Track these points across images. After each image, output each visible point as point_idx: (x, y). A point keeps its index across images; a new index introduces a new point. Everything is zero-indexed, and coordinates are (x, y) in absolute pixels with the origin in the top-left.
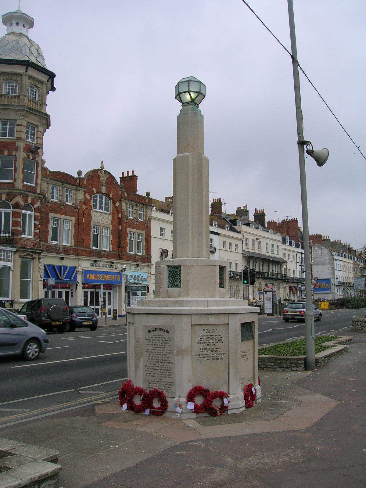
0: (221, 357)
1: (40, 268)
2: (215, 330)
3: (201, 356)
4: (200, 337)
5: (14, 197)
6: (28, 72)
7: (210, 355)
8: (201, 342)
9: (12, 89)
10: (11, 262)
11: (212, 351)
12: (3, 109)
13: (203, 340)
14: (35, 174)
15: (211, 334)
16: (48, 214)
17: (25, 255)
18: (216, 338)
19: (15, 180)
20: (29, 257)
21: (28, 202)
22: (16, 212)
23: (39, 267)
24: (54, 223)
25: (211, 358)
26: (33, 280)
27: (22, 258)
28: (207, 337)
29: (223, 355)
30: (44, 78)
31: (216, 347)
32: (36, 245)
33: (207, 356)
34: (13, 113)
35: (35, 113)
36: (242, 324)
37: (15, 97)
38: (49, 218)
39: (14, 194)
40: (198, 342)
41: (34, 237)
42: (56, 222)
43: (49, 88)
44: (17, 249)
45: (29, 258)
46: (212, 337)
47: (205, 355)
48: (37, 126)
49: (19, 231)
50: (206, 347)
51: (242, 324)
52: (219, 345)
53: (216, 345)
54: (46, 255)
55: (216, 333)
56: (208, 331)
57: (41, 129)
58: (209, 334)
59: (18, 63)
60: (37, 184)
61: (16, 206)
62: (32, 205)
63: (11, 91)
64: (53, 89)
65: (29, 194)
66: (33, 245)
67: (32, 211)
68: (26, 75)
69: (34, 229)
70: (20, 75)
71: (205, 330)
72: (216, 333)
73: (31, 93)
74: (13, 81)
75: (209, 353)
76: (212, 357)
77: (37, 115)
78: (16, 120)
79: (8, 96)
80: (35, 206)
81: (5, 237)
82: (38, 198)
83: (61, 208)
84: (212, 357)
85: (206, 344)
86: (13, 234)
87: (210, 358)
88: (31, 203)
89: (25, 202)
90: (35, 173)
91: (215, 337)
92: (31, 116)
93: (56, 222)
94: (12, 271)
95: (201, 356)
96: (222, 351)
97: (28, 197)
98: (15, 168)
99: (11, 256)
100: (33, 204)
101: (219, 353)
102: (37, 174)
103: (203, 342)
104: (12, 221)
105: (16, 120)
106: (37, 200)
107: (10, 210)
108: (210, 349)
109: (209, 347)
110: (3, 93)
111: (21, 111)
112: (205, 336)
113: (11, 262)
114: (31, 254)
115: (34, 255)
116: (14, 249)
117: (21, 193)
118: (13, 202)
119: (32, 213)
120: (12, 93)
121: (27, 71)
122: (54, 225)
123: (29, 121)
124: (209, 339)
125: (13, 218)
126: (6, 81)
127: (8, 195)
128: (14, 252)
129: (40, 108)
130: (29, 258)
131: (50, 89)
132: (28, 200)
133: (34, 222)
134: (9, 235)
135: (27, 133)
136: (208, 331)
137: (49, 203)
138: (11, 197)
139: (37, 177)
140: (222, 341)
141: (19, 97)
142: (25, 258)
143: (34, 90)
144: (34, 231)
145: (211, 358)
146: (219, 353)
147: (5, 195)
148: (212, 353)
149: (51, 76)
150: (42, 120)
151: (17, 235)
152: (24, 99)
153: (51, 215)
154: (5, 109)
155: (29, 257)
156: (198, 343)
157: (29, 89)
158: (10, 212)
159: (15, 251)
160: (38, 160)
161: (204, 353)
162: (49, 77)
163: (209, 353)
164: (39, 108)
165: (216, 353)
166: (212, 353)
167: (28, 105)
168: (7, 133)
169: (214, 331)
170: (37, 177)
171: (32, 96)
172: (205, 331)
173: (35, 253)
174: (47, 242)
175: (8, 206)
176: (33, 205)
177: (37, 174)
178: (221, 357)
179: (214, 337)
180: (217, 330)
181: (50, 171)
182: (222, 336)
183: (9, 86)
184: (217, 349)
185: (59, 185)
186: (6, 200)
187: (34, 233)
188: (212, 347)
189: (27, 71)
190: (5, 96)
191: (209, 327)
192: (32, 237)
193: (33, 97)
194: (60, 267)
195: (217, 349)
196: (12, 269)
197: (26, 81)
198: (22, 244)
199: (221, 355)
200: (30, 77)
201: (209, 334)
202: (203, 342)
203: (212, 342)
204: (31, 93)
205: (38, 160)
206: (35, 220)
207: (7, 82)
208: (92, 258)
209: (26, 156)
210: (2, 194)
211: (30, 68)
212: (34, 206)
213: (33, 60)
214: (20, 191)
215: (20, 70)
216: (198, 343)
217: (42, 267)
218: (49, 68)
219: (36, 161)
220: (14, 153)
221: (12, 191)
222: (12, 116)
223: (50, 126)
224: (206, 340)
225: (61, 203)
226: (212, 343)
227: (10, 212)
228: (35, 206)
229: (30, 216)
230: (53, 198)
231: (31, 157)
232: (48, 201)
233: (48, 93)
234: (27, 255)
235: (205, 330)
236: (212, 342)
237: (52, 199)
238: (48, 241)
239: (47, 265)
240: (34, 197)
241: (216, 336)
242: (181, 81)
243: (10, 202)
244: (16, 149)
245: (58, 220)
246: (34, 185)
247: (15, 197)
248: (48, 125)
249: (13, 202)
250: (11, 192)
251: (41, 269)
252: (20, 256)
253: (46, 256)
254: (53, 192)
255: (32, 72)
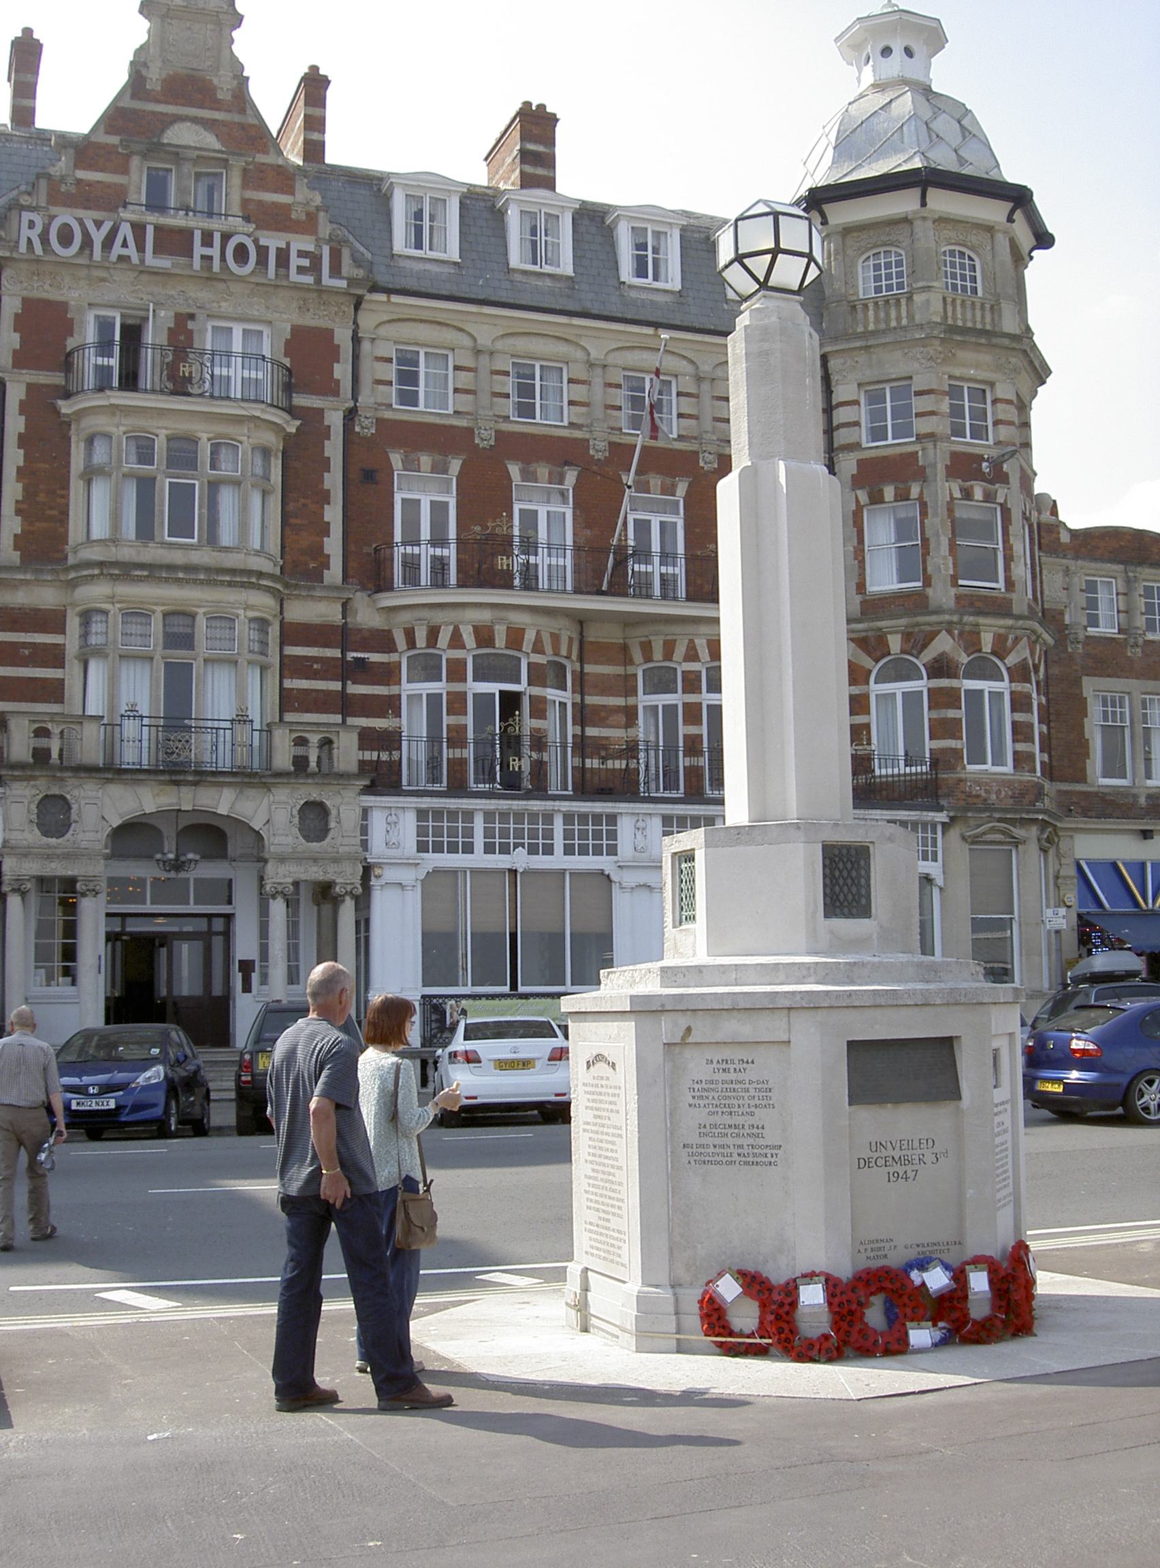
0: (769, 1155)
1: (1062, 873)
2: (747, 1062)
3: (700, 1150)
4: (696, 1086)
5: (930, 637)
6: (830, 222)
7: (732, 1150)
8: (702, 1102)
9: (889, 277)
10: (935, 859)
11: (738, 1135)
12: (861, 348)
13: (707, 1098)
14: (1001, 549)
15: (733, 1076)
16: (1077, 683)
17: (984, 833)
18: (752, 1092)
19: (927, 582)
20: (999, 837)
21: (980, 651)
22: (941, 689)
23: (1058, 871)
24: (1105, 713)
25: (735, 1157)
26: (1020, 917)
27: (973, 843)
28: (720, 1086)
29: (774, 1151)
30: (993, 211)
31: (750, 1120)
32: (1022, 795)
33: (722, 1151)
34: (898, 354)
35: (974, 339)
36: (851, 1045)
37: (898, 301)
38: (1085, 695)
39: (928, 628)
40: (692, 1101)
41: (1014, 767)
42: (1114, 706)
43: (1024, 236)
44: (952, 814)
45: (1000, 843)
46: (736, 1087)
47: (715, 1146)
48: (992, 385)
49: (957, 753)
50: (717, 1119)
51: (851, 1045)
52: (762, 1116)
53: (752, 1114)
54: (1082, 826)
55: (751, 1074)
56: (724, 1066)
57: (1004, 390)
58: (725, 1076)
59: (854, 191)
60: (1010, 584)
61: (940, 668)
62: (998, 657)
63: (884, 283)
64: (1044, 240)
65: (982, 620)
66: (1011, 797)
67: (1003, 680)
68: (924, 219)
69: (1014, 741)
70: (906, 221)
71: (715, 1062)
72: (751, 1074)
73: (954, 276)
74: (888, 249)
75: (729, 1141)
76: (739, 1155)
77: (981, 344)
78: (910, 378)
79: (876, 303)
80: (1012, 660)
81: (914, 777)
82: (1019, 632)
83: (1129, 654)
84: (739, 1155)
85: (717, 1109)
86: (935, 763)
87: (729, 1159)
88: (994, 653)
89: (971, 650)
90: (1000, 546)
91: (747, 1086)
92: (962, 354)
93: (1114, 706)
94: (941, 889)
95: (700, 1150)
96: (771, 1138)
97: (979, 633)
98: (925, 541)
99: (934, 840)
100: (1000, 650)
101: (761, 1142)
102: (1008, 547)
103: (707, 1102)
104: (930, 719)
105: (910, 378)
106: (1017, 640)
107: (920, 685)
108: (730, 1126)
109: (728, 1120)
110: (861, 297)
111: (923, 342)
112: (712, 1082)
113: (935, 859)
114: (1005, 825)
115: (1019, 832)
116: (942, 817)
117: (950, 623)
118: (929, 654)
119: (1003, 686)
120: (889, 288)
121: (924, 204)
122: (1105, 719)
123: (957, 372)
124: (727, 1094)
125: (932, 711)
126: (863, 253)
127: (907, 636)
128: (943, 824)
129: (993, 320)
130: (1000, 843)
131: (1033, 242)
132: (980, 643)
133: (1012, 717)
134: (924, 770)
135: (957, 411)
136: (724, 1066)
137: (1078, 642)
138: (917, 641)
139: (1008, 559)
140: (771, 1102)
141: (910, 299)
142: (986, 843)
143: (967, 261)
144: (1013, 747)
145: (735, 1157)
146: (761, 1142)
147: (899, 636)
148: (739, 1141)
149: (1020, 198)
150: (1003, 360)
151: (952, 768)
152: (928, 301)
153: (1090, 687)
154: (867, 348)
155: (999, 837)
156: (690, 1105)
157: (945, 261)
158: (922, 691)
159: (947, 820)
160: (1006, 500)
161: (709, 1141)
162: (1010, 205)
163: (729, 1141)
164: (988, 319)
165: (751, 1141)
166: (739, 1141)
167: (945, 317)
168: (886, 426)
169: (745, 1065)
170: (1008, 559)
171: (959, 282)
172: (715, 1064)
173: (1023, 822)
174: (1082, 779)
175: (912, 674)
176: (1002, 659)
177: (1008, 547)
178: (769, 1155)
179: (743, 1086)
180: (753, 1062)
181: (1070, 531)
182: (770, 1086)
183: (877, 267)
184: (755, 1131)
185: (1116, 574)
186: (903, 652)
187: (1015, 753)
188: (739, 1120)
189: (924, 204)
190: (866, 306)
191: (727, 1053)
192: (1009, 768)
193: (964, 288)
194: (1143, 865)
195: (755, 1131)
196: (940, 881)
197: (925, 235)
198: (970, 795)
199: (768, 1151)
200: (943, 221)
201: (725, 1076)
202: (707, 1102)
203: (735, 1102)
204: (954, 276)
205: (1006, 500)
206: (1013, 710)
207: (869, 257)
208: (1118, 824)
209: (957, 494)
210: (891, 633)
211: (932, 193)
212: (1006, 661)
213: (945, 160)
214: (947, 617)
215: (903, 203)
216: (690, 1105)
217: (1073, 872)
218: (1011, 174)
219: (1001, 505)
220: (915, 491)
221: (920, 619)
222: (896, 364)
223: (1048, 372)
224: (716, 1095)
225: (1125, 639)
226: (736, 1109)
227: (922, 691)
228: (1012, 660)
229: (996, 696)
230: (1093, 621)
231: (978, 494)
232: (1074, 636)
233: (1020, 260)
234: (993, 830)
235: (715, 1062)
236: (735, 1102)
237: (1089, 629)
238: (1086, 775)
239: (1123, 863)
240: (1002, 631)
241: (751, 1082)
242: (748, 210)
243: (917, 658)
244: (921, 474)
245: (1121, 699)
246: (1001, 585)
247: (932, 639)
248: (1040, 373)
249: (929, 654)
250: (918, 625)
251: (1065, 878)
252: (964, 838)
253: (1081, 829)
254: (1093, 604)
255: (943, 202)
